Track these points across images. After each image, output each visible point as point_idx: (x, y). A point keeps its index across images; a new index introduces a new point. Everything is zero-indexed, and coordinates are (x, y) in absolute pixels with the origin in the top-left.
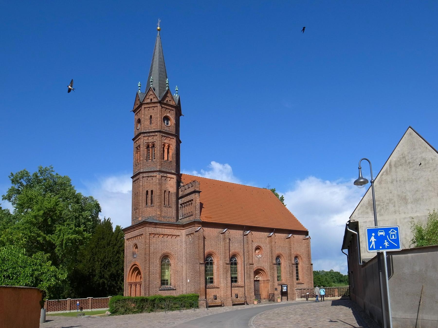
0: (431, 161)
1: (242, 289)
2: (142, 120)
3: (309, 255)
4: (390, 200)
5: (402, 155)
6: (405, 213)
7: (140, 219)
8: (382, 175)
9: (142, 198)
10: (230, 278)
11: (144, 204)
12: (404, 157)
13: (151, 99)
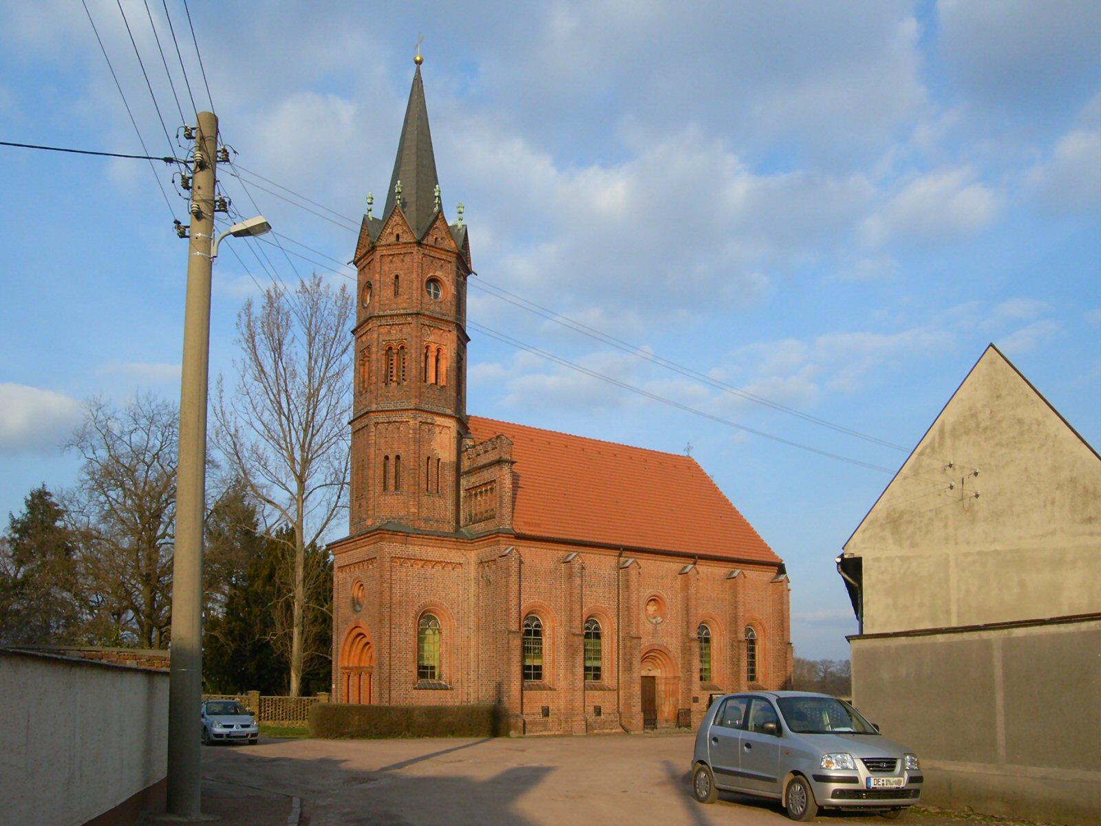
0: (1035, 427)
1: (612, 696)
2: (376, 286)
3: (782, 621)
4: (937, 511)
5: (970, 409)
6: (968, 543)
7: (369, 522)
8: (921, 454)
9: (375, 474)
10: (582, 670)
11: (379, 489)
12: (974, 415)
13: (398, 236)
